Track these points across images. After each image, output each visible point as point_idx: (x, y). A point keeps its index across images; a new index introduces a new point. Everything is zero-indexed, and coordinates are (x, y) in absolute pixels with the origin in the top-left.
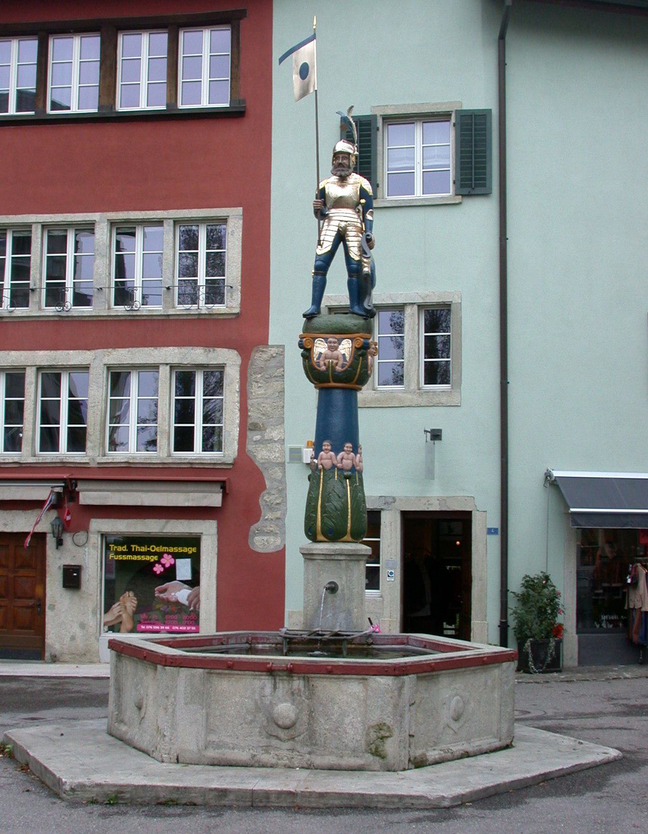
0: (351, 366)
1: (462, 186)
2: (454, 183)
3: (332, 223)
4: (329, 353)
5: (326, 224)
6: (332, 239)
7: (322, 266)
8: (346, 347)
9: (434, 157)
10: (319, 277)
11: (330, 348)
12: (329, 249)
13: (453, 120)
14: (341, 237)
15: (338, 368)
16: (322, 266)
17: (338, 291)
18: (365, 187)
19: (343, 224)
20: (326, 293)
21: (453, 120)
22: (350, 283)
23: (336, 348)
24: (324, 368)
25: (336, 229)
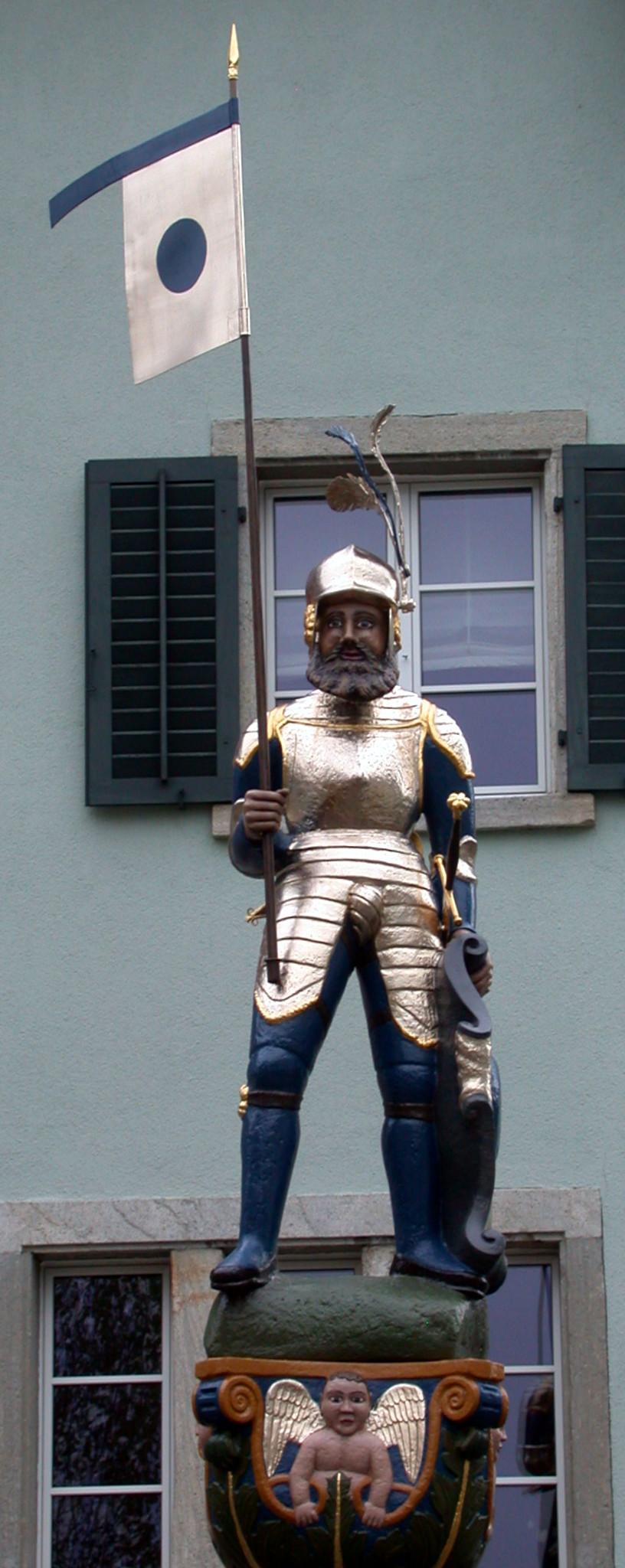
0: (426, 1500)
1: (597, 755)
2: (563, 740)
3: (319, 888)
4: (331, 1440)
5: (289, 893)
6: (321, 953)
7: (281, 1070)
8: (400, 1416)
9: (460, 636)
10: (273, 1116)
11: (331, 1421)
12: (310, 997)
13: (553, 484)
14: (357, 948)
15: (373, 1510)
16: (281, 1070)
17: (343, 1182)
18: (445, 743)
19: (368, 893)
20: (302, 1186)
21: (553, 484)
22: (393, 1146)
23: (358, 1421)
24: (307, 1508)
25: (337, 912)
